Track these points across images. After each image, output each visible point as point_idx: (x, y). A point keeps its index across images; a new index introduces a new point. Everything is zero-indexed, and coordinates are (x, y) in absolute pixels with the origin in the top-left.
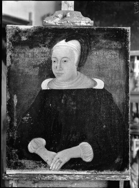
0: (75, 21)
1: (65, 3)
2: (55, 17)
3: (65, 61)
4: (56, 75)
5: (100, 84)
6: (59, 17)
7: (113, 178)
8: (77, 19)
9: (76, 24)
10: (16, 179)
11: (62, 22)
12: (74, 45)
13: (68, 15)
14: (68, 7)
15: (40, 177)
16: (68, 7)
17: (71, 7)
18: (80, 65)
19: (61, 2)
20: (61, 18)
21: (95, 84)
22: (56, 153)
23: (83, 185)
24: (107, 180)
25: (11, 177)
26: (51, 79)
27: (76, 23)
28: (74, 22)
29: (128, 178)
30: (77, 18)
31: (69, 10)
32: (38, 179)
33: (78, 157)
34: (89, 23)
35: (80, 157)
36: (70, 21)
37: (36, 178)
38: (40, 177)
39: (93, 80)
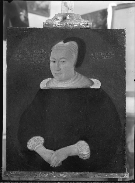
0: (74, 23)
1: (65, 6)
2: (55, 20)
3: (63, 62)
4: (54, 75)
5: (97, 84)
6: (59, 19)
7: (111, 176)
8: (77, 22)
9: (75, 25)
10: (18, 176)
11: (62, 24)
12: (73, 45)
13: (68, 17)
14: (68, 10)
15: (40, 175)
16: (68, 10)
17: (70, 10)
18: (78, 65)
19: (131, 96)
20: (61, 21)
21: (92, 83)
22: (54, 150)
23: (63, 175)
24: (106, 177)
25: (12, 174)
26: (50, 79)
27: (75, 24)
28: (73, 24)
29: (127, 176)
30: (77, 20)
31: (69, 13)
32: (38, 176)
33: (76, 155)
34: (87, 24)
35: (77, 155)
36: (69, 23)
37: (37, 175)
38: (40, 175)
39: (90, 79)
